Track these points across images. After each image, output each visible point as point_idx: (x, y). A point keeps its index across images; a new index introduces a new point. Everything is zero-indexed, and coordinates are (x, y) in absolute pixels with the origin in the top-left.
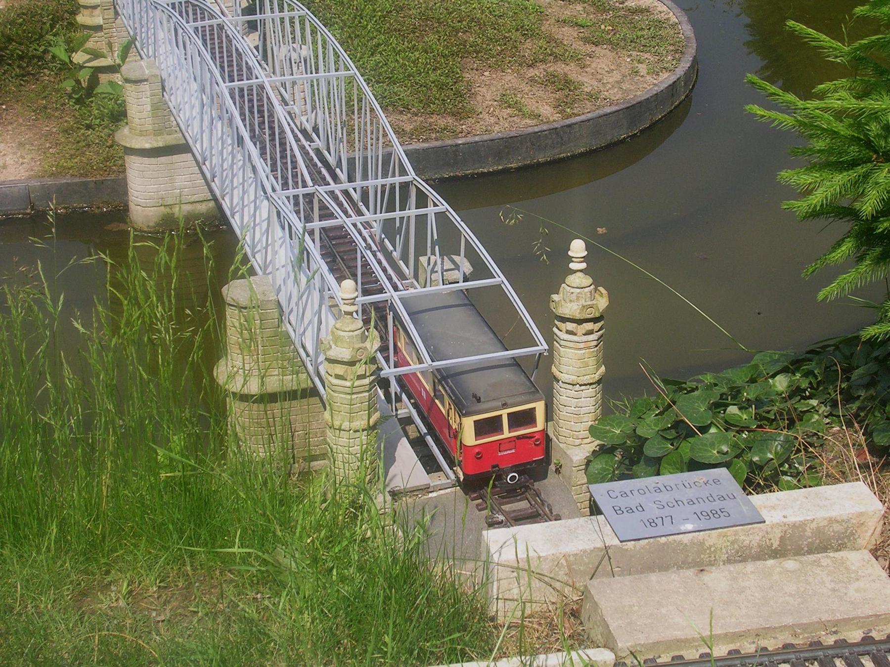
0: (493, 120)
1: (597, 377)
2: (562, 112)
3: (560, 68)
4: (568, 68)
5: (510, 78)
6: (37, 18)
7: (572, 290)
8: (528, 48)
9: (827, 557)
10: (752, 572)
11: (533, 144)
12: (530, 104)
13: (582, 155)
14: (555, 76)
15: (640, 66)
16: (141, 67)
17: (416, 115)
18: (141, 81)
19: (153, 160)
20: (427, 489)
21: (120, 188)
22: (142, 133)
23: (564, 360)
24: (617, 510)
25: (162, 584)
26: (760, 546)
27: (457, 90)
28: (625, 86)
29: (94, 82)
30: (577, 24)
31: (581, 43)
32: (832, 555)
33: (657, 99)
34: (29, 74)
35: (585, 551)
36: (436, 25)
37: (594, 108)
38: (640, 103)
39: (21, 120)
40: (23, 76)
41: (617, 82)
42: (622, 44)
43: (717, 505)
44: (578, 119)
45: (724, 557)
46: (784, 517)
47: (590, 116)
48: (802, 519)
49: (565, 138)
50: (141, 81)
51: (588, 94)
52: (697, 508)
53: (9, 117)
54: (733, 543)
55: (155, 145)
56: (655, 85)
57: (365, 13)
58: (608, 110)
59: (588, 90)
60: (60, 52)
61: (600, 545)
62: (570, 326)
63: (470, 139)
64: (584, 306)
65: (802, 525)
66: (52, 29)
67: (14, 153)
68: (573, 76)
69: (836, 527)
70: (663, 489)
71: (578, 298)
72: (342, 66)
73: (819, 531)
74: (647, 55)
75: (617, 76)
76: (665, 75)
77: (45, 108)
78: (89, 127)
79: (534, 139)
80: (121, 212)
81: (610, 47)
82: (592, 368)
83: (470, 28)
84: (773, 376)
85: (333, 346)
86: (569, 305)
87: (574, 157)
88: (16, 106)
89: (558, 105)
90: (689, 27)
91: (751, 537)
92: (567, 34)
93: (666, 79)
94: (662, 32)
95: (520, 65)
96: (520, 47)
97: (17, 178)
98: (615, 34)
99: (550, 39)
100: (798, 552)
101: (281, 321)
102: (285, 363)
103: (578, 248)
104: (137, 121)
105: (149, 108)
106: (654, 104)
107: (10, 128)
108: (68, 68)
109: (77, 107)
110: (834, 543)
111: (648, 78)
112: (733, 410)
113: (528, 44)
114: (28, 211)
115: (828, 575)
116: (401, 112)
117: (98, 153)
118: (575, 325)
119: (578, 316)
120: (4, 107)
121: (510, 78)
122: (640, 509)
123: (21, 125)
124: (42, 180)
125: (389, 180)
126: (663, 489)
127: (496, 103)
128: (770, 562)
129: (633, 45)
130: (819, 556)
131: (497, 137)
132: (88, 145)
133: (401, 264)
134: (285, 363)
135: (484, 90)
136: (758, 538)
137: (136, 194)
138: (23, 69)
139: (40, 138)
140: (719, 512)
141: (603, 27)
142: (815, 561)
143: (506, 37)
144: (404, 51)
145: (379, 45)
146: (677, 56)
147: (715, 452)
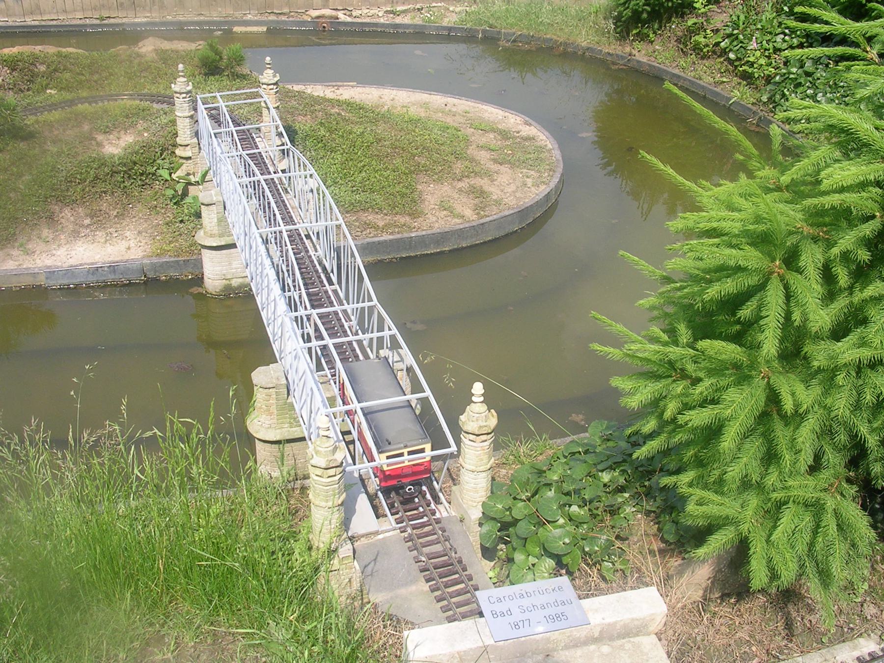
0: (435, 219)
1: (488, 466)
2: (478, 214)
3: (478, 182)
4: (483, 181)
5: (446, 188)
7: (474, 415)
8: (459, 167)
9: (630, 641)
10: (580, 656)
11: (459, 236)
12: (459, 209)
13: (490, 241)
14: (474, 188)
15: (528, 180)
16: (211, 195)
17: (387, 215)
18: (211, 205)
19: (219, 252)
20: (377, 533)
21: (199, 264)
22: (212, 236)
23: (467, 456)
24: (494, 614)
25: (197, 640)
26: (586, 637)
27: (413, 198)
28: (518, 195)
29: (185, 193)
30: (489, 149)
31: (492, 163)
32: (632, 639)
33: (538, 204)
34: (146, 184)
35: (471, 649)
36: (401, 152)
37: (498, 211)
38: (527, 208)
39: (141, 215)
40: (143, 185)
41: (514, 192)
42: (517, 164)
43: (560, 609)
44: (488, 219)
45: (563, 644)
46: (603, 619)
47: (495, 217)
48: (614, 620)
49: (480, 232)
50: (211, 205)
51: (495, 201)
52: (547, 612)
53: (133, 213)
54: (569, 637)
55: (220, 244)
56: (537, 195)
57: (357, 144)
58: (507, 213)
59: (494, 197)
60: (165, 174)
61: (481, 644)
62: (472, 437)
63: (420, 233)
64: (481, 427)
65: (616, 623)
66: (161, 156)
67: (136, 239)
68: (486, 188)
69: (636, 623)
70: (525, 595)
71: (477, 420)
73: (625, 626)
74: (532, 173)
75: (513, 187)
76: (543, 187)
77: (156, 207)
78: (182, 221)
79: (460, 233)
80: (199, 280)
81: (509, 166)
82: (485, 461)
83: (422, 153)
84: (602, 471)
85: (315, 455)
86: (471, 423)
87: (485, 243)
88: (138, 205)
89: (477, 209)
90: (559, 152)
91: (581, 633)
92: (483, 156)
93: (543, 190)
94: (542, 156)
95: (453, 180)
96: (454, 166)
97: (136, 257)
98: (513, 157)
99: (472, 160)
100: (611, 638)
101: (288, 394)
102: (292, 421)
103: (478, 388)
104: (208, 228)
105: (216, 221)
106: (535, 208)
107: (134, 220)
108: (169, 183)
109: (175, 207)
110: (634, 631)
111: (533, 189)
112: (574, 508)
113: (459, 165)
114: (143, 278)
115: (629, 657)
116: (377, 213)
118: (475, 436)
119: (477, 433)
120: (131, 206)
121: (446, 189)
122: (509, 613)
123: (140, 218)
124: (151, 258)
125: (361, 305)
126: (525, 595)
127: (437, 207)
128: (592, 647)
129: (524, 164)
130: (624, 641)
131: (436, 232)
132: (181, 235)
133: (368, 350)
134: (292, 421)
135: (429, 197)
136: (585, 633)
139: (152, 228)
140: (561, 616)
141: (506, 151)
142: (621, 646)
143: (444, 160)
144: (381, 170)
145: (364, 166)
146: (551, 173)
147: (561, 543)
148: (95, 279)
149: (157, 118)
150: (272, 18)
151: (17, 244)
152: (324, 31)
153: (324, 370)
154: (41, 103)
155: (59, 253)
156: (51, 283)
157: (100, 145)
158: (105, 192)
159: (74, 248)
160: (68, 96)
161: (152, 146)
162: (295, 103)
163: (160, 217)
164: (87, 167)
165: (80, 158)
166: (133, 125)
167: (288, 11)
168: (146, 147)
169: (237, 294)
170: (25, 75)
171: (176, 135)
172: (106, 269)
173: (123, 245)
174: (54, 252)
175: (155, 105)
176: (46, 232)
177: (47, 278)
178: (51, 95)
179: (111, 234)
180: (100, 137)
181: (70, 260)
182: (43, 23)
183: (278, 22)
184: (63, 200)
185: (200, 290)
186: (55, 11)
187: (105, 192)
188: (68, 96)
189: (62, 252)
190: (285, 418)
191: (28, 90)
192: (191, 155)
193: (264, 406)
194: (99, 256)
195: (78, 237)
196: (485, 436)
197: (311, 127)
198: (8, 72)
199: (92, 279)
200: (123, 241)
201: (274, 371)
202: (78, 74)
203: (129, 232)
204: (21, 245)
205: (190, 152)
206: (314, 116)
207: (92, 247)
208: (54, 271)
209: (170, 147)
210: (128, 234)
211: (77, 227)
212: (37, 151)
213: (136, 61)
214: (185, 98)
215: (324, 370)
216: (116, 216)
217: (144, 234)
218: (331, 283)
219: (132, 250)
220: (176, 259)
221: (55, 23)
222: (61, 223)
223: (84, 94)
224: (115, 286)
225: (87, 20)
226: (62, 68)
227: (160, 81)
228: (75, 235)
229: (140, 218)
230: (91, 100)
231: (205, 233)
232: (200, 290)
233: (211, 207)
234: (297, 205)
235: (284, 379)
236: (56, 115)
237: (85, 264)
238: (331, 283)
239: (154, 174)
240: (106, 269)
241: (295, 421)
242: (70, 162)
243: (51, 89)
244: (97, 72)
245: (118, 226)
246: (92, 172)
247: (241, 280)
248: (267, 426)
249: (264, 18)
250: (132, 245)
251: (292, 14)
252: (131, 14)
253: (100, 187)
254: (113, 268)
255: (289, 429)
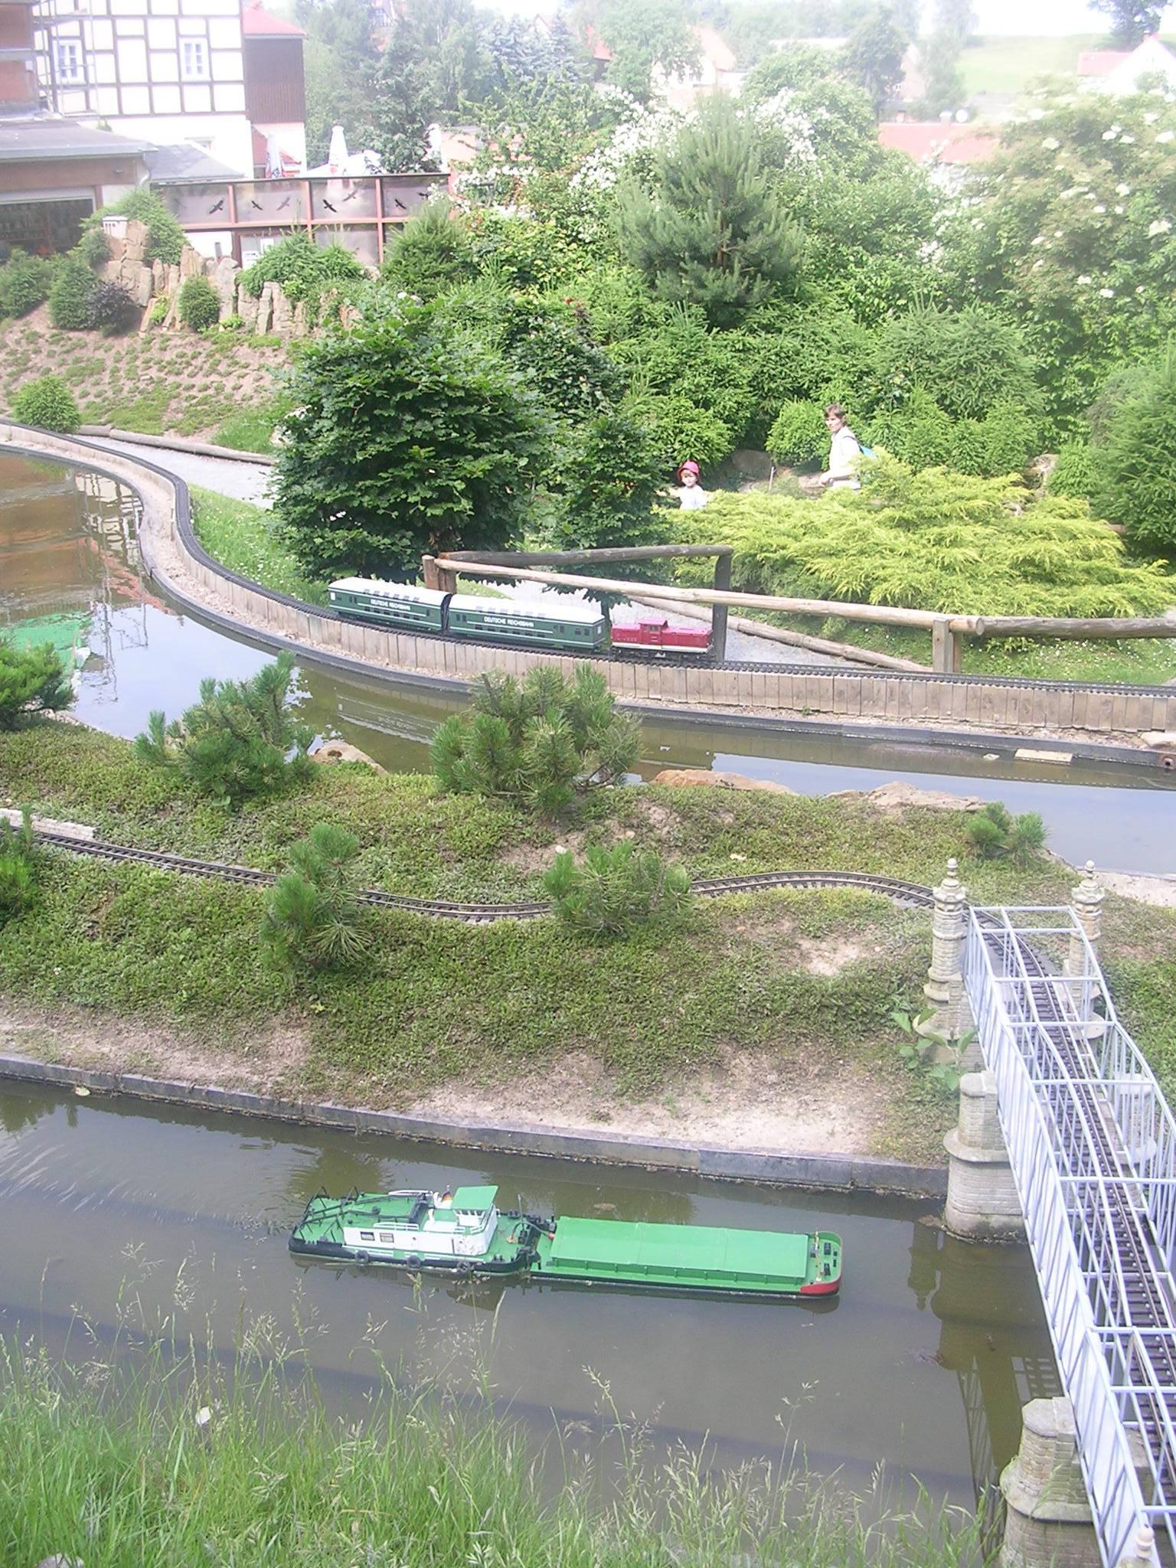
6: (886, 977)
18: (978, 1097)
22: (971, 1144)
34: (870, 1029)
39: (855, 1079)
40: (864, 1031)
50: (978, 1097)
55: (982, 1159)
60: (900, 1019)
67: (844, 1118)
72: (1110, 1088)
77: (881, 1069)
80: (937, 1204)
88: (852, 1063)
105: (981, 1122)
107: (844, 1086)
114: (848, 1186)
117: (924, 1137)
123: (854, 1084)
132: (916, 1125)
134: (1074, 1493)
137: (955, 1198)
138: (866, 1024)
148: (774, 1175)
149: (898, 923)
150: (1082, 739)
151: (662, 1098)
152: (1167, 770)
153: (1136, 1420)
154: (721, 874)
155: (723, 1123)
156: (706, 1169)
157: (805, 957)
158: (804, 1035)
159: (747, 1119)
160: (763, 867)
161: (887, 972)
162: (1119, 922)
163: (885, 1089)
164: (783, 992)
165: (774, 976)
166: (859, 931)
167: (1109, 729)
168: (878, 972)
169: (995, 1239)
170: (702, 828)
171: (928, 960)
172: (794, 1162)
173: (825, 1125)
174: (717, 1120)
175: (895, 901)
176: (707, 1086)
177: (702, 1161)
178: (736, 863)
179: (807, 1104)
180: (806, 944)
181: (740, 1138)
182: (715, 710)
183: (1091, 748)
184: (739, 1040)
185: (936, 1222)
186: (735, 693)
187: (804, 1035)
188: (763, 867)
189: (729, 1122)
190: (1064, 1486)
191: (703, 851)
192: (947, 998)
193: (1033, 1462)
194: (786, 1139)
195: (756, 1100)
196: (828, 657)
197: (1143, 968)
198: (678, 820)
199: (769, 1174)
200: (825, 1120)
201: (1058, 1410)
202: (782, 833)
203: (834, 1106)
204: (669, 1102)
205: (948, 994)
206: (1149, 947)
207: (775, 1121)
208: (715, 1153)
209: (915, 977)
210: (833, 1108)
211: (756, 1084)
212: (709, 956)
213: (870, 821)
214: (952, 911)
215: (1136, 1420)
216: (817, 1075)
217: (858, 1112)
218: (1160, 1268)
219: (838, 1137)
220: (905, 1165)
221: (731, 712)
222: (732, 1075)
223: (787, 867)
224: (804, 1191)
225: (783, 711)
226: (757, 821)
227: (906, 858)
228: (752, 1097)
229: (854, 1084)
230: (798, 879)
231: (961, 1137)
232: (936, 1222)
233: (977, 1101)
234: (1114, 1116)
235: (1074, 1426)
236: (742, 899)
237: (763, 1149)
238: (1160, 1268)
239: (883, 1016)
240: (794, 1162)
241: (1081, 1494)
242: (758, 981)
243: (738, 852)
244: (810, 833)
245: (819, 1092)
246: (790, 1001)
247: (1005, 1219)
248: (1032, 1492)
249: (1068, 739)
250: (838, 1129)
251: (1115, 733)
252: (854, 709)
253: (799, 1026)
254: (805, 1163)
255: (1066, 1504)
